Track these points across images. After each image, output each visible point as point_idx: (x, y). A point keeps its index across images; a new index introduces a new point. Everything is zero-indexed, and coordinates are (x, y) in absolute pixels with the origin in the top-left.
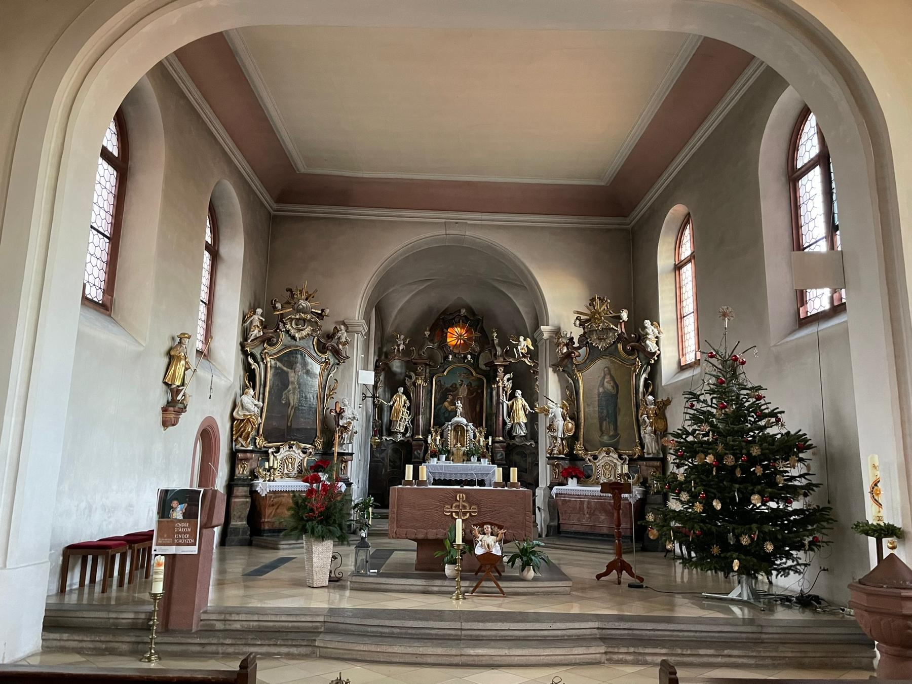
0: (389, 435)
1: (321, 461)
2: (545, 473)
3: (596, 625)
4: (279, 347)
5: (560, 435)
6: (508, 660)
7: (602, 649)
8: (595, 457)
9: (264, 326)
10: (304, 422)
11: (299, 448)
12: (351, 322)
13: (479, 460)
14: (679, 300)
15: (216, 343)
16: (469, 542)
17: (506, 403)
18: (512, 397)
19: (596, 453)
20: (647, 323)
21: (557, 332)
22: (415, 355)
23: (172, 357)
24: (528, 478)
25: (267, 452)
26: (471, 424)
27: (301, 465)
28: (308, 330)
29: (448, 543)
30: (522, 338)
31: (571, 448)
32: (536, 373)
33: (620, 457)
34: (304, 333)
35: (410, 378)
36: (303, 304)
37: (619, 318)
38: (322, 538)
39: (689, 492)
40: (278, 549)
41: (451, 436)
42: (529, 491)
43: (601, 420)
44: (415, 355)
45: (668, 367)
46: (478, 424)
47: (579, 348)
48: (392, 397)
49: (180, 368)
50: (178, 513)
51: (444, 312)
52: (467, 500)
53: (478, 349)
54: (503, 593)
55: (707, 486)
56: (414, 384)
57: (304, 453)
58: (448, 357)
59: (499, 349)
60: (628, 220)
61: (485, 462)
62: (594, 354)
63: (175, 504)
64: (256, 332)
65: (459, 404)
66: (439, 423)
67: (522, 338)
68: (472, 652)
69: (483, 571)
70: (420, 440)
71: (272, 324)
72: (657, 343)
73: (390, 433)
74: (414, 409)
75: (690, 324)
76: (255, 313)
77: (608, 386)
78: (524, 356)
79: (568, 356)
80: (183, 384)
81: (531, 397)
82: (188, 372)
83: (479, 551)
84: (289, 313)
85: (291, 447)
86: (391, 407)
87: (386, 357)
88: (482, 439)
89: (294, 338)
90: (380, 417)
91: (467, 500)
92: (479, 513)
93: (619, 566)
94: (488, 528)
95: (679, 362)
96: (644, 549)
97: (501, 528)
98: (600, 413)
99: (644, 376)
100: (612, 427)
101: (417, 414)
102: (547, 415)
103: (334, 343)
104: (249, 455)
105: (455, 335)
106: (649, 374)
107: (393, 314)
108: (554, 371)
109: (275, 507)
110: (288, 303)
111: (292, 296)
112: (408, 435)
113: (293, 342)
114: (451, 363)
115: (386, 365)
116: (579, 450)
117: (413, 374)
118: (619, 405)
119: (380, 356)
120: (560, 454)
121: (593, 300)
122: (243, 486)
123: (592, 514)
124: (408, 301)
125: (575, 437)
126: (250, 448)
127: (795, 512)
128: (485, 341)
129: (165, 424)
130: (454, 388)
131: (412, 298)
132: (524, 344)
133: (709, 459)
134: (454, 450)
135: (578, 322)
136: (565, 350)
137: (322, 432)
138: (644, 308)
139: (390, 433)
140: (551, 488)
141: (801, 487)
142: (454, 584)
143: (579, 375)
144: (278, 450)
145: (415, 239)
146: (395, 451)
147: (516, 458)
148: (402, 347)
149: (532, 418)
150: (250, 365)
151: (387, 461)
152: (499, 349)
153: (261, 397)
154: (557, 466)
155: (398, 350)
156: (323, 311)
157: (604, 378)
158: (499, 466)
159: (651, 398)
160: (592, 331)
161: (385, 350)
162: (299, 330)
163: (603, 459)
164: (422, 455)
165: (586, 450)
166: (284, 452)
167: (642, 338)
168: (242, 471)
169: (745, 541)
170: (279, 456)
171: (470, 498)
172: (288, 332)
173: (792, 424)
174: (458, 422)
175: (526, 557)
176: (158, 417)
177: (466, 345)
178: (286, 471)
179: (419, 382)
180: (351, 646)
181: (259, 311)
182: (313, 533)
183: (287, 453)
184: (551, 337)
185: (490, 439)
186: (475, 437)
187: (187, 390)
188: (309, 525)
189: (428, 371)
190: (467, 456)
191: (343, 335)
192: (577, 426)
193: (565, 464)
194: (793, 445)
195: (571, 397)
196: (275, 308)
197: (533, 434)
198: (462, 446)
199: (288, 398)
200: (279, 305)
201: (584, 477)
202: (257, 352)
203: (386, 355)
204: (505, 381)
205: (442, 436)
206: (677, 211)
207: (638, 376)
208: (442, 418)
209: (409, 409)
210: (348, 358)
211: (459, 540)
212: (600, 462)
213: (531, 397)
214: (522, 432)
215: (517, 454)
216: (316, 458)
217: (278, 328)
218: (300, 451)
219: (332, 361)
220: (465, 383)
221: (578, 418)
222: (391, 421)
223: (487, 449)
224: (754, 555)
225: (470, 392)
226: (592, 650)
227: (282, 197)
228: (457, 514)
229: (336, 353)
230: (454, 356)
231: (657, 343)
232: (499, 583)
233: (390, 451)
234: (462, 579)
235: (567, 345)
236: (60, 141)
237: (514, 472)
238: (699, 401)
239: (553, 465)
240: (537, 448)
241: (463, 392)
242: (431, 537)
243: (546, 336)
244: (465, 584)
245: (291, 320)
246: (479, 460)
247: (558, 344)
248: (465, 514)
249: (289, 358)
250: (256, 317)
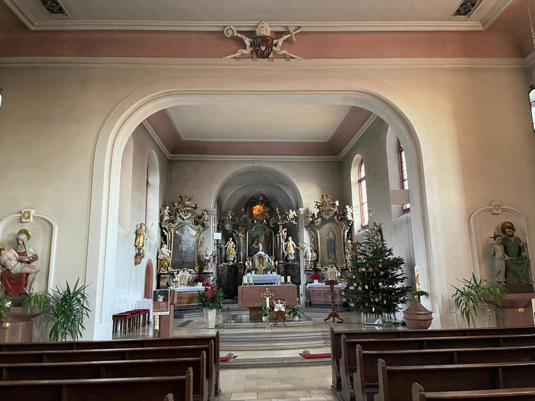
0: (226, 262)
1: (199, 277)
2: (303, 278)
3: (321, 334)
4: (177, 224)
5: (310, 259)
6: (289, 347)
7: (323, 342)
8: (326, 270)
9: (170, 215)
10: (189, 259)
11: (188, 271)
12: (209, 210)
13: (271, 273)
14: (361, 196)
16: (272, 307)
17: (284, 244)
18: (287, 240)
19: (327, 267)
20: (347, 207)
21: (307, 211)
22: (237, 221)
23: (137, 234)
24: (296, 280)
25: (173, 274)
26: (267, 255)
28: (190, 215)
29: (263, 308)
30: (291, 211)
31: (315, 266)
32: (298, 228)
33: (337, 269)
34: (188, 217)
35: (235, 232)
36: (188, 203)
37: (335, 204)
38: (212, 308)
39: (356, 283)
40: (183, 318)
41: (257, 261)
42: (295, 286)
43: (328, 252)
44: (237, 221)
45: (357, 227)
46: (270, 255)
47: (317, 218)
48: (226, 243)
49: (141, 239)
50: (161, 299)
51: (251, 199)
52: (270, 290)
53: (269, 217)
54: (286, 326)
55: (363, 280)
56: (237, 235)
58: (254, 221)
59: (279, 216)
60: (338, 157)
61: (275, 274)
62: (324, 221)
63: (159, 296)
64: (166, 218)
65: (261, 245)
66: (251, 255)
67: (291, 211)
68: (276, 344)
69: (278, 318)
70: (241, 264)
71: (174, 213)
72: (352, 216)
73: (226, 261)
74: (238, 249)
75: (365, 206)
76: (165, 209)
77: (331, 236)
78: (292, 220)
79: (312, 222)
80: (143, 246)
81: (296, 240)
82: (145, 240)
83: (276, 310)
84: (181, 208)
86: (226, 248)
87: (223, 222)
88: (273, 262)
89: (183, 219)
90: (221, 253)
91: (270, 290)
92: (275, 295)
93: (334, 315)
94: (279, 301)
95: (362, 225)
96: (348, 310)
97: (284, 301)
98: (328, 248)
99: (347, 231)
100: (333, 255)
101: (239, 251)
102: (303, 251)
103: (201, 220)
104: (166, 276)
105: (257, 209)
106: (349, 230)
107: (225, 201)
108: (306, 229)
110: (180, 203)
111: (182, 199)
114: (256, 224)
115: (223, 226)
116: (319, 266)
117: (236, 231)
118: (336, 245)
119: (219, 222)
120: (310, 268)
121: (323, 196)
123: (325, 296)
124: (233, 194)
125: (317, 260)
126: (167, 272)
127: (398, 289)
128: (272, 213)
129: (136, 264)
130: (258, 237)
132: (292, 214)
133: (364, 269)
134: (259, 268)
135: (316, 207)
136: (311, 220)
137: (198, 263)
138: (345, 200)
139: (226, 261)
140: (306, 284)
141: (400, 279)
142: (266, 324)
143: (318, 231)
144: (178, 272)
145: (238, 169)
146: (229, 270)
147: (289, 271)
148: (230, 217)
149: (297, 251)
150: (164, 233)
151: (225, 275)
152: (279, 216)
153: (169, 248)
154: (309, 274)
156: (196, 205)
157: (329, 232)
158: (282, 275)
159: (350, 241)
160: (323, 211)
161: (222, 219)
162: (186, 215)
163: (330, 270)
165: (322, 266)
166: (181, 273)
167: (345, 214)
168: (163, 283)
169: (377, 300)
171: (271, 290)
172: (180, 216)
173: (396, 254)
174: (260, 254)
175: (294, 311)
176: (133, 260)
177: (262, 214)
179: (240, 234)
180: (231, 345)
181: (168, 208)
182: (208, 306)
184: (304, 214)
185: (277, 262)
186: (269, 261)
187: (144, 248)
188: (206, 303)
190: (266, 271)
191: (206, 217)
192: (318, 255)
193: (313, 273)
194: (397, 263)
195: (314, 242)
196: (174, 206)
197: (298, 259)
198: (263, 266)
199: (182, 248)
200: (176, 204)
201: (321, 279)
202: (167, 227)
203: (223, 221)
204: (283, 233)
205: (252, 262)
206: (358, 157)
207: (344, 231)
208: (252, 252)
211: (268, 306)
212: (328, 272)
213: (296, 240)
214: (292, 258)
215: (291, 269)
217: (176, 215)
219: (201, 229)
220: (263, 234)
221: (318, 252)
222: (226, 255)
223: (275, 267)
224: (381, 305)
225: (266, 239)
226: (319, 342)
227: (174, 151)
228: (266, 296)
229: (203, 225)
230: (257, 221)
231: (352, 216)
232: (285, 323)
233: (226, 271)
234: (270, 322)
235: (312, 217)
236: (110, 158)
237: (289, 278)
238: (361, 246)
239: (307, 274)
240: (300, 265)
241: (262, 238)
242: (256, 306)
243: (302, 213)
244: (271, 323)
245: (182, 211)
246: (271, 273)
247: (308, 217)
248: (269, 296)
249: (181, 227)
250: (166, 211)
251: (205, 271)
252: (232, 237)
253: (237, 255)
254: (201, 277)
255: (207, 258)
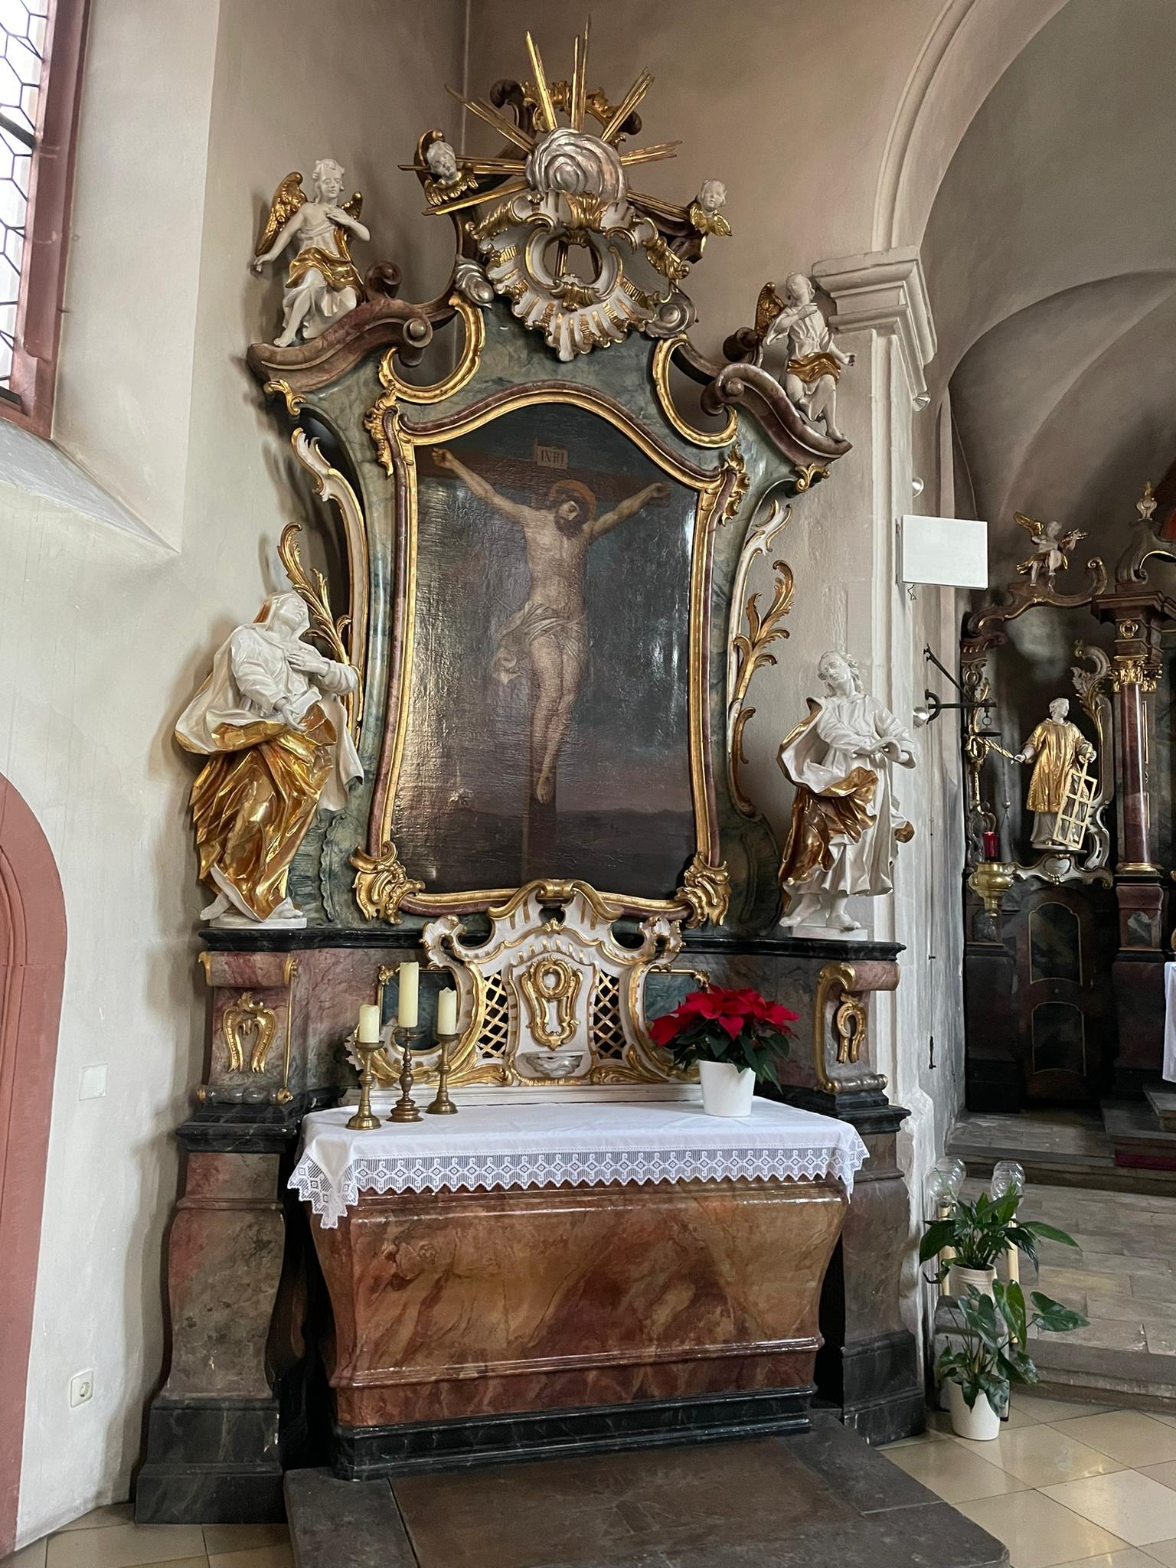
0: (1026, 864)
4: (461, 379)
11: (595, 915)
15: (95, 348)
27: (609, 1004)
35: (1090, 667)
48: (1026, 735)
56: (1106, 686)
57: (629, 940)
70: (1144, 878)
73: (1027, 855)
74: (1114, 775)
85: (553, 910)
86: (1026, 770)
89: (537, 340)
109: (417, 1292)
112: (1094, 861)
113: (540, 371)
115: (999, 625)
117: (1098, 655)
122: (242, 1145)
131: (1085, 384)
137: (724, 833)
148: (1054, 560)
151: (1024, 947)
155: (1043, 574)
162: (571, 300)
164: (1156, 933)
166: (517, 935)
170: (482, 966)
178: (526, 1044)
183: (536, 943)
189: (1155, 637)
202: (341, 404)
209: (1093, 770)
210: (839, 448)
216: (704, 969)
218: (604, 933)
219: (760, 468)
229: (776, 423)
233: (1032, 917)
251: (801, 922)
252: (1070, 693)
253: (1109, 816)
254: (753, 1002)
255: (816, 779)
